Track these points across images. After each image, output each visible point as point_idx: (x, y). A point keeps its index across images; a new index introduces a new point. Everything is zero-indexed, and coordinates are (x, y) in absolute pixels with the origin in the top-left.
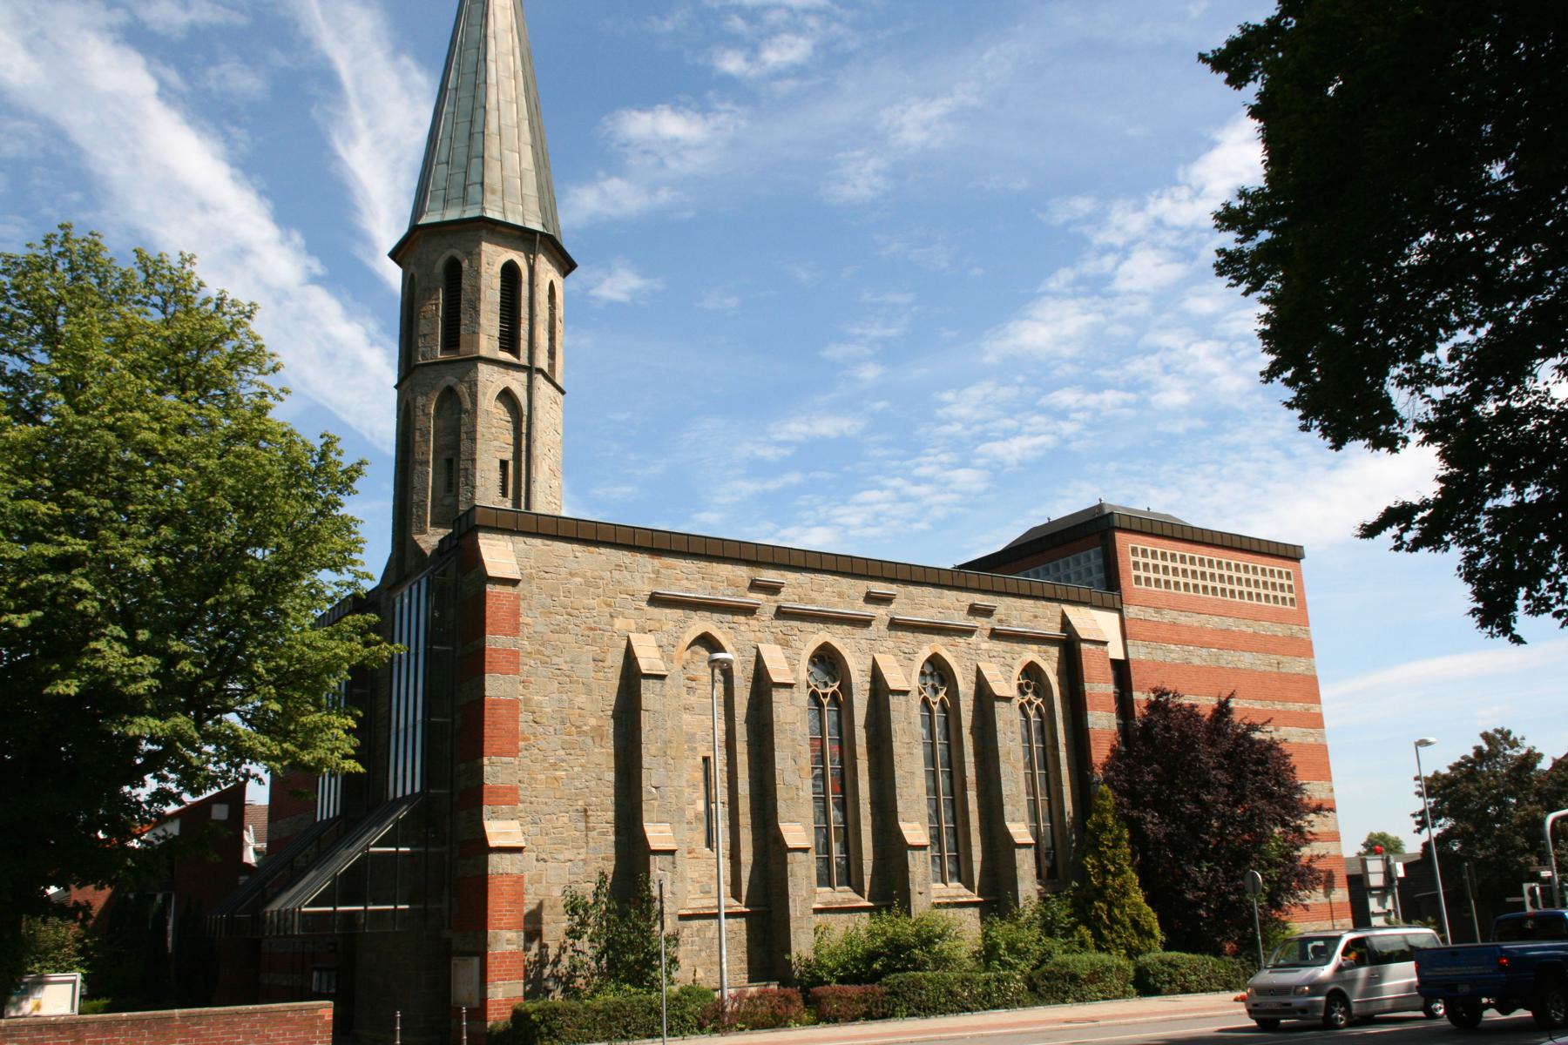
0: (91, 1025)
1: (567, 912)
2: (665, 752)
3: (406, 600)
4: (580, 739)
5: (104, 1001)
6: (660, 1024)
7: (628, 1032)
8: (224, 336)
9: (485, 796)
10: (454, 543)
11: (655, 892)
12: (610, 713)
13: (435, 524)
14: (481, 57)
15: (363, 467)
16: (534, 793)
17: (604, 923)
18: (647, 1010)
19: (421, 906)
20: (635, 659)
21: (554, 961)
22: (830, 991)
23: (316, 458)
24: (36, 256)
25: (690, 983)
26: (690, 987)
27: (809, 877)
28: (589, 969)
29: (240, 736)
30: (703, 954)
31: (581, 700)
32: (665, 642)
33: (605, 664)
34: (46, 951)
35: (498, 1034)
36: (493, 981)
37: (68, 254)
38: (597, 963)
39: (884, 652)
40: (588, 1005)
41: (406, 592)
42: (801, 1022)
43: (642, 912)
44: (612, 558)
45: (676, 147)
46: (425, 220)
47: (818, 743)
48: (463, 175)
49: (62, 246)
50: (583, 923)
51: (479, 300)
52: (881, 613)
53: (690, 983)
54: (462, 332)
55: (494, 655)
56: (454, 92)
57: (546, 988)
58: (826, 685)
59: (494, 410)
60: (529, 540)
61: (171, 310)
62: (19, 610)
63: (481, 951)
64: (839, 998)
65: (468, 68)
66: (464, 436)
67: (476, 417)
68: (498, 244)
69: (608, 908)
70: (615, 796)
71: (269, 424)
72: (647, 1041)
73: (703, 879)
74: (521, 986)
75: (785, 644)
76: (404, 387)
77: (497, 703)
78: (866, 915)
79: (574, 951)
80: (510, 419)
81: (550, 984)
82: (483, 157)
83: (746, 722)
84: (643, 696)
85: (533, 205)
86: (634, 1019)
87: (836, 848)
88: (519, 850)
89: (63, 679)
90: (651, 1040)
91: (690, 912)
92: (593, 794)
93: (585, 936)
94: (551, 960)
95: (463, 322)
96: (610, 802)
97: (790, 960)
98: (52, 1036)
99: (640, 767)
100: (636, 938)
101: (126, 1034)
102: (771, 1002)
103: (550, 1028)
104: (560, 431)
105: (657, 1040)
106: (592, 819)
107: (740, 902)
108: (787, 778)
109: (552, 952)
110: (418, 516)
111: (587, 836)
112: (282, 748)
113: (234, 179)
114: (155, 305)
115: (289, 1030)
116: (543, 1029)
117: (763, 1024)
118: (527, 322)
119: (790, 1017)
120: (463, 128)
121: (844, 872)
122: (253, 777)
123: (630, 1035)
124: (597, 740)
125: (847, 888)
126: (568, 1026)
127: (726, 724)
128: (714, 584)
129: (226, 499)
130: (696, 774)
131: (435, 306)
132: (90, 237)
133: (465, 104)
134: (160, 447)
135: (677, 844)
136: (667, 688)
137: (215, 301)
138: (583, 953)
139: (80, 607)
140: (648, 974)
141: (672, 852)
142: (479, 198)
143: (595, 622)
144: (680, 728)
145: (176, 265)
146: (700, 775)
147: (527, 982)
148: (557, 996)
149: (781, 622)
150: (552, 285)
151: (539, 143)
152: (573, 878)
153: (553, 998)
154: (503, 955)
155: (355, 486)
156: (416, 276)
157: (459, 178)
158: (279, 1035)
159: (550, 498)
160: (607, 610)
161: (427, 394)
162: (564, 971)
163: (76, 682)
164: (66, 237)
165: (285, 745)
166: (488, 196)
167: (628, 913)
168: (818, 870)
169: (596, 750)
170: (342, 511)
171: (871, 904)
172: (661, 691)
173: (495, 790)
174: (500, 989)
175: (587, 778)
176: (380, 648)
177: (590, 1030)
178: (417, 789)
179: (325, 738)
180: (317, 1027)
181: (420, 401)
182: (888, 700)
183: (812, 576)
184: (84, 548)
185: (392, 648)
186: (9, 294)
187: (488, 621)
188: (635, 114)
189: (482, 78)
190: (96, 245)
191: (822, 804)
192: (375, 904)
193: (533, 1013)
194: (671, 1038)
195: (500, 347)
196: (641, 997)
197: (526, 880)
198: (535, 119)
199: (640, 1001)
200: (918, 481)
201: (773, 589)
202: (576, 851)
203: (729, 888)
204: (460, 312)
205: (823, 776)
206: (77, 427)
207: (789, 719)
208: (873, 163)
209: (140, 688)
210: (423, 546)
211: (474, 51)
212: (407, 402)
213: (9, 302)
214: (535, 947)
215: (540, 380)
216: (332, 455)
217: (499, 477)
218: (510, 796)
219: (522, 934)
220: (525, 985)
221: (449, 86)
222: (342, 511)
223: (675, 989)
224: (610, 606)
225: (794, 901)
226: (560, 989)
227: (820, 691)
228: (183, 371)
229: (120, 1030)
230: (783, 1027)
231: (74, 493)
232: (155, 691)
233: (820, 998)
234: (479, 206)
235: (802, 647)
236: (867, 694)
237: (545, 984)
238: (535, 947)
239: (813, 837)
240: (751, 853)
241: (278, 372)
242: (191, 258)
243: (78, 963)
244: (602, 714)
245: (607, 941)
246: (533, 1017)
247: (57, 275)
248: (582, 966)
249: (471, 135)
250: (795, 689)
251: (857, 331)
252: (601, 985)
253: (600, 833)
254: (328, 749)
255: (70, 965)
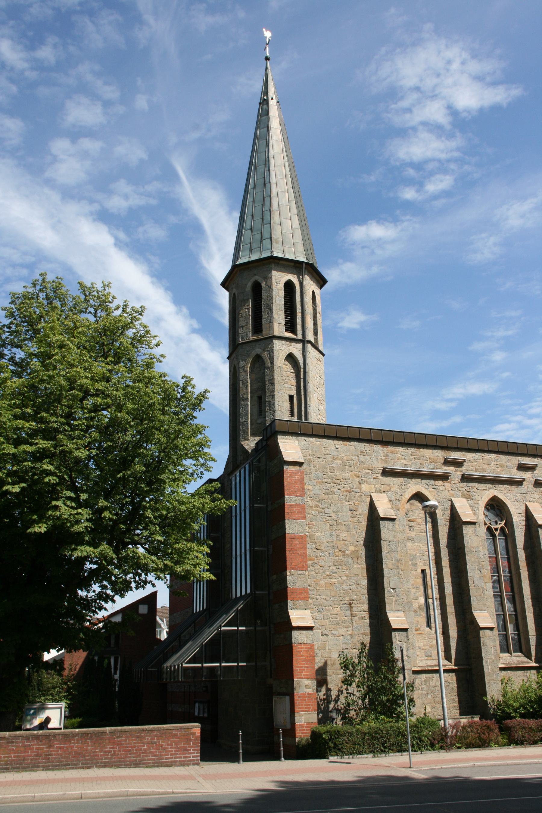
0: (57, 737)
1: (342, 668)
2: (398, 566)
3: (238, 479)
4: (345, 559)
5: (78, 720)
6: (407, 743)
7: (385, 747)
8: (126, 326)
9: (289, 594)
10: (264, 443)
11: (397, 655)
12: (362, 543)
13: (253, 434)
14: (267, 169)
15: (207, 394)
16: (318, 593)
17: (366, 675)
18: (397, 733)
19: (253, 664)
20: (376, 508)
21: (335, 699)
22: (516, 723)
23: (180, 391)
24: (28, 292)
25: (422, 715)
26: (423, 718)
27: (495, 647)
28: (357, 705)
29: (139, 557)
30: (429, 696)
31: (344, 535)
32: (393, 498)
33: (358, 513)
34: (48, 689)
35: (303, 746)
36: (298, 712)
37: (45, 289)
38: (363, 701)
39: (533, 501)
40: (359, 729)
41: (238, 474)
42: (502, 745)
43: (389, 668)
44: (359, 448)
45: (380, 242)
46: (239, 262)
47: (494, 560)
48: (260, 234)
49: (41, 285)
50: (352, 675)
51: (272, 303)
52: (528, 476)
53: (422, 715)
54: (263, 323)
55: (290, 508)
56: (252, 190)
57: (331, 717)
58: (496, 523)
59: (284, 366)
60: (308, 439)
61: (99, 315)
62: (13, 483)
63: (290, 692)
64: (524, 728)
65: (260, 176)
66: (267, 382)
67: (274, 371)
68: (281, 271)
69: (367, 666)
70: (368, 595)
71: (153, 373)
72: (398, 754)
73: (426, 647)
74: (316, 716)
75: (468, 497)
76: (232, 358)
77: (293, 538)
78: (534, 672)
79: (347, 693)
80: (293, 371)
81: (334, 715)
82: (270, 223)
83: (447, 547)
84: (382, 532)
85: (300, 248)
86: (389, 739)
87: (511, 628)
88: (310, 628)
89: (38, 524)
90: (400, 754)
91: (419, 669)
92: (354, 593)
93: (354, 684)
94: (333, 698)
95: (263, 317)
96: (365, 598)
97: (487, 701)
98: (35, 743)
99: (383, 576)
100: (387, 685)
101: (78, 743)
102: (477, 729)
103: (335, 744)
104: (323, 377)
105: (404, 753)
106: (354, 609)
107: (451, 663)
108: (476, 582)
109: (334, 693)
110: (243, 430)
111: (352, 619)
112: (164, 564)
113: (153, 283)
114: (90, 313)
115: (174, 742)
116: (331, 744)
117: (473, 744)
118: (300, 314)
119: (491, 740)
120: (259, 209)
121: (517, 644)
122: (149, 583)
123: (387, 750)
124: (355, 559)
125: (520, 654)
126: (347, 743)
127: (435, 548)
128: (422, 461)
129: (128, 414)
130: (418, 580)
131: (248, 310)
132: (56, 280)
133: (259, 196)
134: (91, 387)
135: (409, 625)
136: (396, 527)
137: (122, 307)
138: (354, 695)
139: (46, 480)
140: (396, 709)
141: (406, 630)
142: (269, 247)
143: (350, 487)
144: (406, 551)
145: (100, 289)
146: (420, 581)
147: (319, 711)
148: (339, 721)
149: (465, 484)
150: (313, 293)
151: (302, 214)
152: (345, 646)
153: (336, 723)
154: (304, 695)
155: (203, 405)
156: (236, 294)
157: (258, 237)
158: (168, 745)
159: (319, 417)
160: (357, 480)
161: (245, 360)
162: (342, 706)
163: (45, 525)
164: (44, 281)
165: (166, 562)
166: (274, 244)
167: (380, 669)
168: (500, 642)
169: (355, 566)
170: (196, 421)
171: (537, 665)
172: (393, 528)
173: (294, 591)
174: (303, 717)
175: (351, 583)
176: (221, 502)
177: (360, 746)
178: (249, 591)
179: (190, 558)
180: (191, 740)
181: (242, 364)
182: (538, 532)
183: (483, 455)
184: (49, 445)
185: (228, 502)
186: (15, 314)
187: (286, 488)
188: (357, 227)
189: (268, 180)
190: (60, 284)
191: (499, 599)
192: (226, 662)
193: (324, 733)
194: (414, 753)
195: (286, 330)
196: (392, 724)
197: (316, 647)
198: (299, 200)
199: (391, 727)
200: (531, 417)
201: (459, 464)
202: (345, 629)
203: (443, 653)
204: (262, 311)
205: (499, 581)
206: (45, 378)
207: (475, 544)
208: (492, 240)
209: (79, 528)
210: (247, 447)
211: (263, 166)
212: (235, 366)
213: (15, 319)
214: (324, 690)
215: (309, 347)
216: (189, 388)
217: (289, 405)
218: (304, 594)
219: (315, 681)
220: (318, 715)
221: (250, 188)
222: (196, 421)
223: (414, 719)
224: (358, 477)
225: (487, 662)
226: (340, 718)
227: (493, 527)
228: (106, 349)
229: (74, 740)
230: (488, 746)
231: (45, 414)
232: (89, 529)
233: (510, 728)
234: (270, 250)
235: (479, 499)
236: (523, 528)
237: (331, 714)
238: (324, 690)
239: (495, 621)
240: (456, 631)
241: (159, 347)
242: (108, 284)
243: (64, 697)
244: (357, 543)
245: (368, 687)
246: (324, 736)
247: (39, 301)
248: (353, 703)
249: (263, 212)
250: (477, 526)
251: (490, 334)
252: (366, 716)
253: (360, 618)
254: (192, 565)
255: (60, 698)
